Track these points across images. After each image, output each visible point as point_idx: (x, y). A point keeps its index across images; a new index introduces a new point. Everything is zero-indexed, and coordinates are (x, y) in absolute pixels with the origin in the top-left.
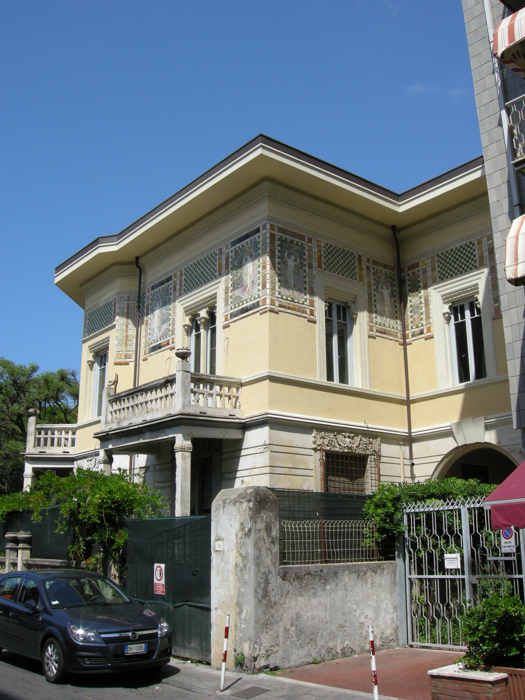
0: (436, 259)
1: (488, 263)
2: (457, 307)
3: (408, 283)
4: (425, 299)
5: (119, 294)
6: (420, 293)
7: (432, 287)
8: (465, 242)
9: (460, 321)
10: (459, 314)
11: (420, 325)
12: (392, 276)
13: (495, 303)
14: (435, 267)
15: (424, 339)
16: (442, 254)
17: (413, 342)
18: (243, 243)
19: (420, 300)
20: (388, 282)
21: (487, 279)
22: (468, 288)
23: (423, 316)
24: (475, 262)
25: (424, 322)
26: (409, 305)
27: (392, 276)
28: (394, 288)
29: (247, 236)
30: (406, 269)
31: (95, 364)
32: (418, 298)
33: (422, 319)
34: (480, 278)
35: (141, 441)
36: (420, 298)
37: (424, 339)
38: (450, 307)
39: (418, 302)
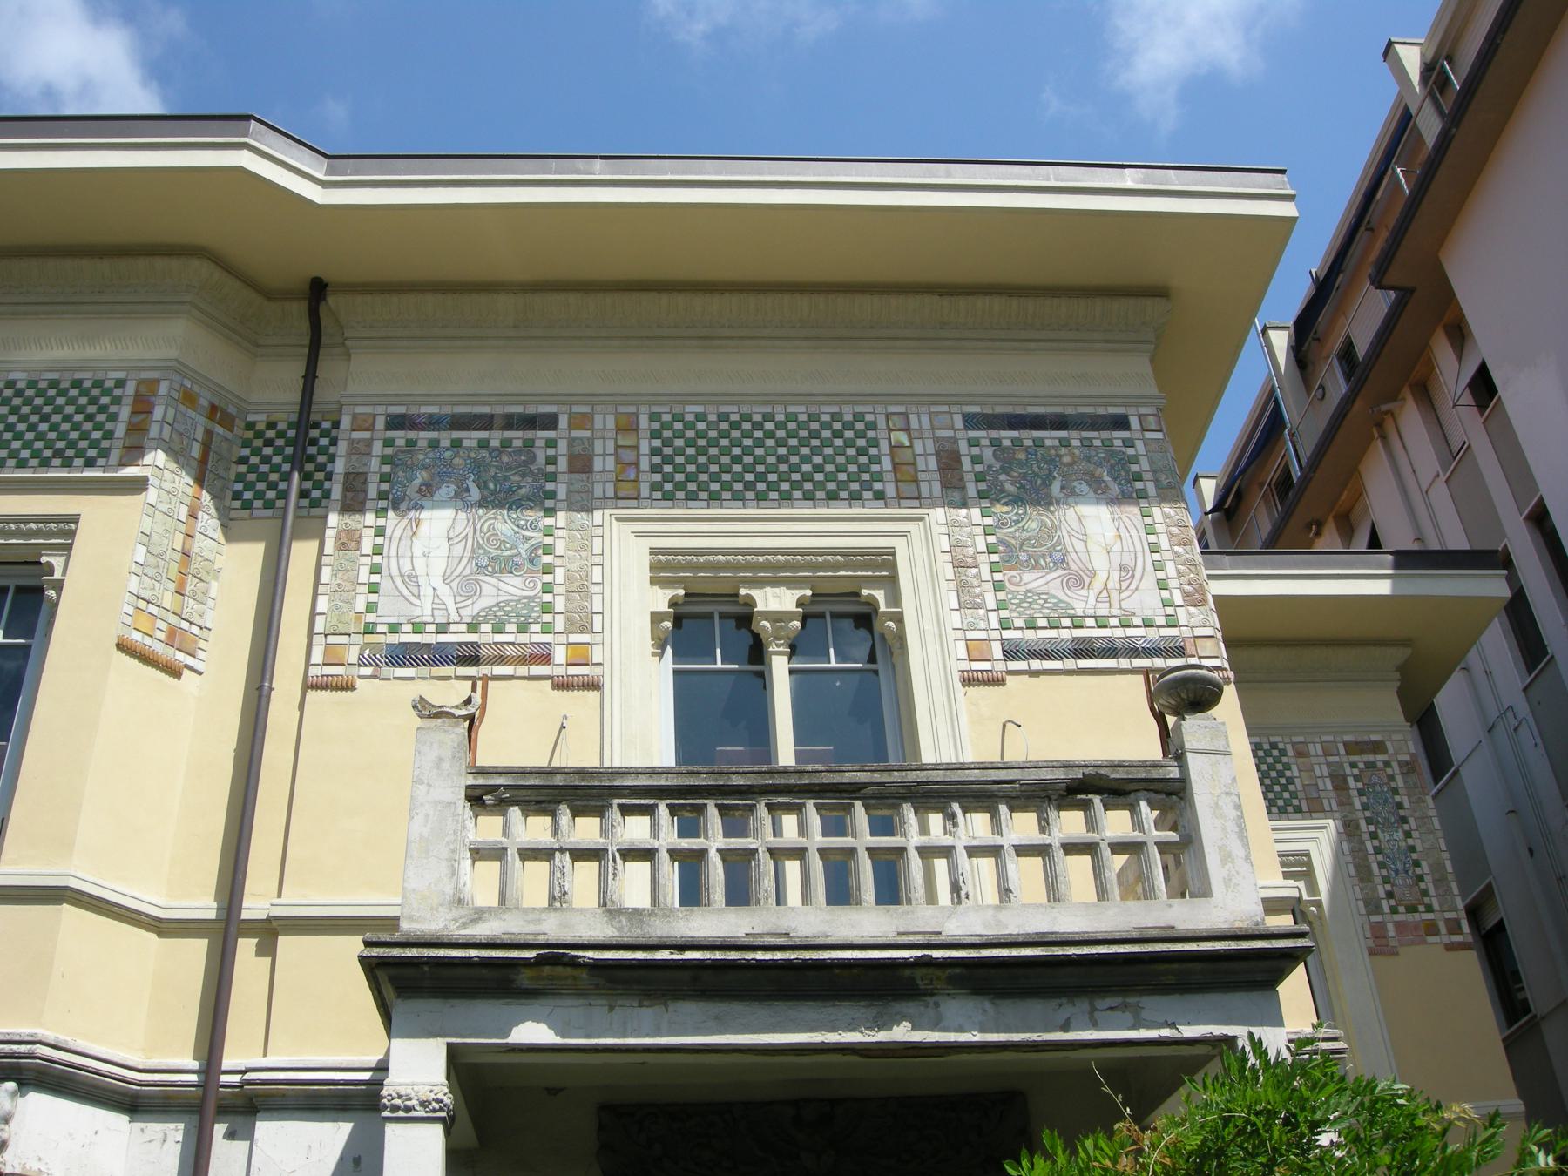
5: (177, 371)
7: (607, 512)
15: (549, 682)
18: (1025, 434)
29: (1037, 423)
31: (1211, 507)
35: (902, 1033)
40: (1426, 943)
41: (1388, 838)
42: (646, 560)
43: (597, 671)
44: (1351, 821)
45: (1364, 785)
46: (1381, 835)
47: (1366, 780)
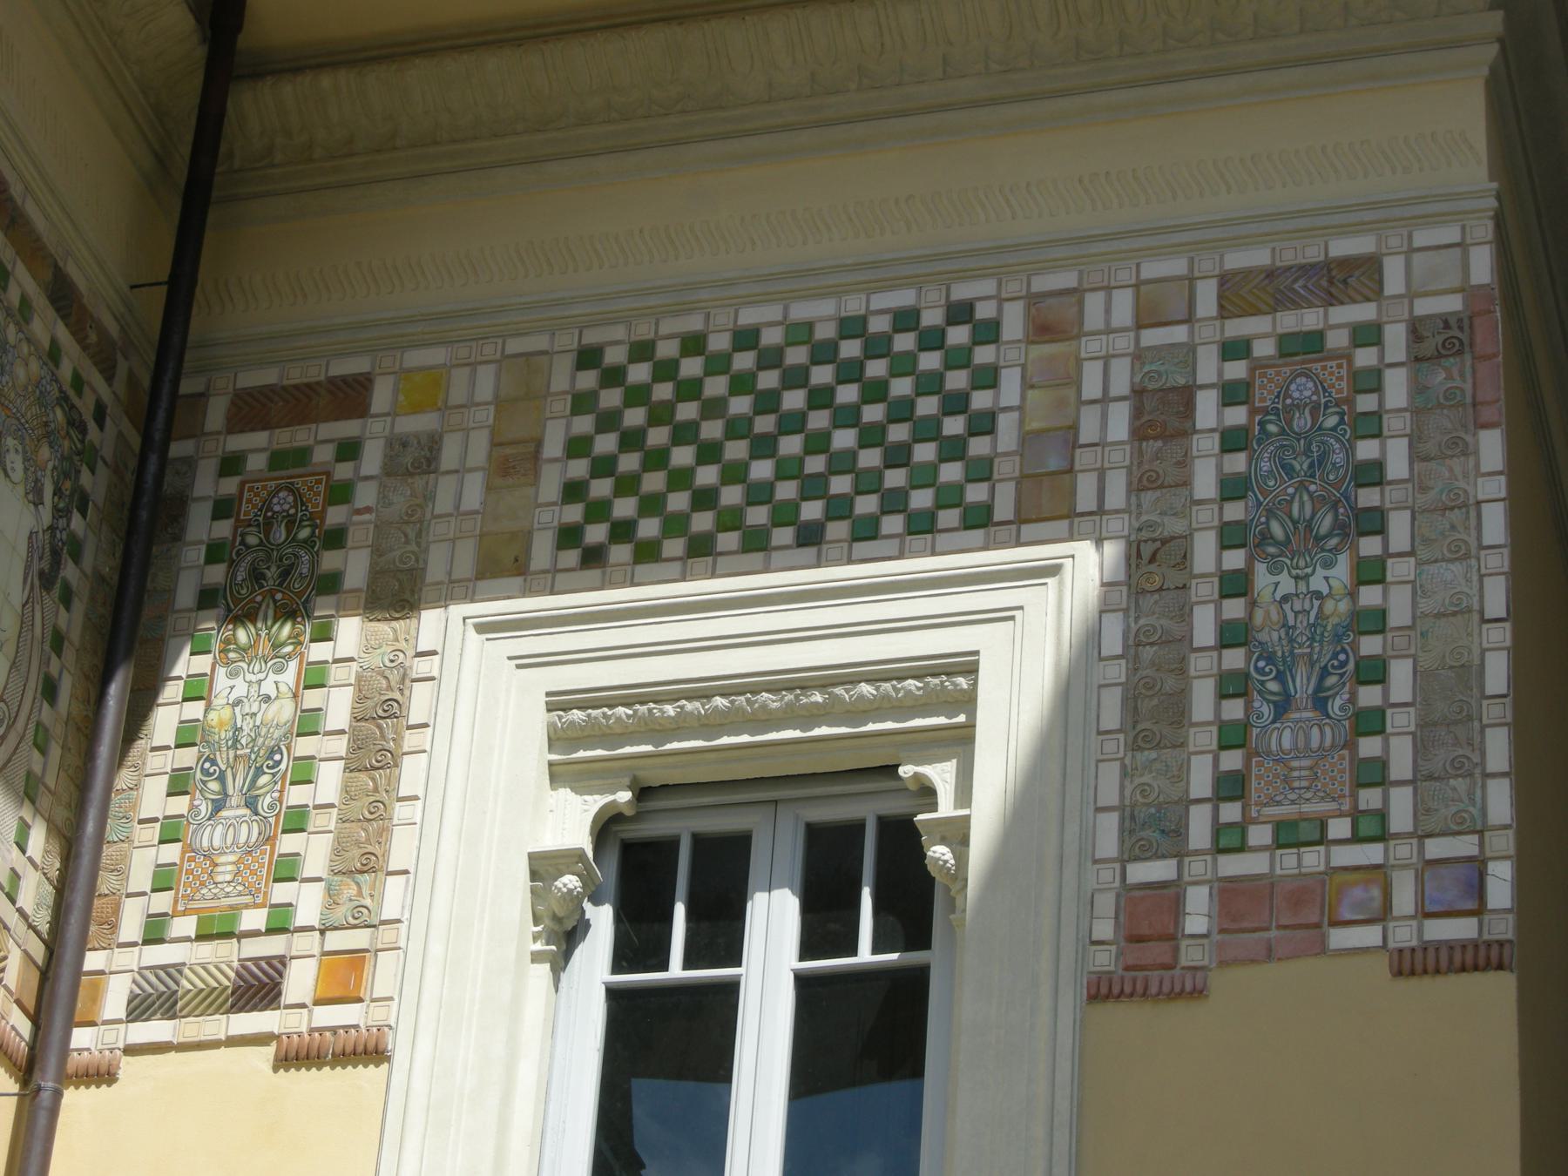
0: (562, 376)
1: (1117, 494)
2: (668, 847)
3: (201, 526)
4: (360, 698)
6: (324, 634)
7: (458, 610)
8: (904, 298)
9: (676, 970)
10: (680, 911)
11: (253, 919)
12: (86, 406)
13: (1135, 848)
14: (539, 443)
15: (270, 1051)
16: (642, 351)
17: (129, 1067)
19: (312, 699)
20: (49, 436)
21: (1091, 640)
22: (853, 681)
23: (315, 851)
24: (982, 471)
25: (308, 904)
26: (164, 722)
27: (86, 406)
28: (77, 523)
30: (216, 413)
32: (289, 676)
33: (287, 870)
34: (1004, 615)
36: (315, 678)
37: (270, 1051)
38: (606, 827)
39: (284, 711)
40: (1322, 949)
41: (1287, 585)
42: (538, 721)
43: (378, 1014)
44: (1164, 542)
45: (1253, 412)
46: (1262, 578)
47: (1264, 396)
